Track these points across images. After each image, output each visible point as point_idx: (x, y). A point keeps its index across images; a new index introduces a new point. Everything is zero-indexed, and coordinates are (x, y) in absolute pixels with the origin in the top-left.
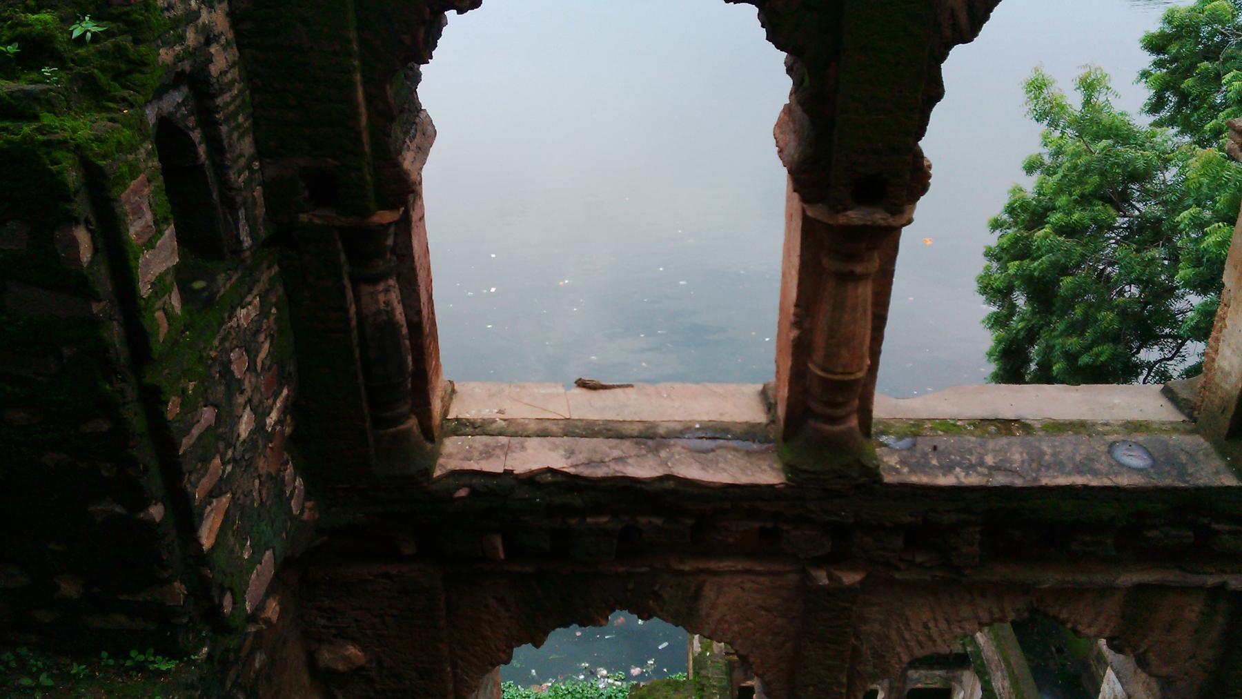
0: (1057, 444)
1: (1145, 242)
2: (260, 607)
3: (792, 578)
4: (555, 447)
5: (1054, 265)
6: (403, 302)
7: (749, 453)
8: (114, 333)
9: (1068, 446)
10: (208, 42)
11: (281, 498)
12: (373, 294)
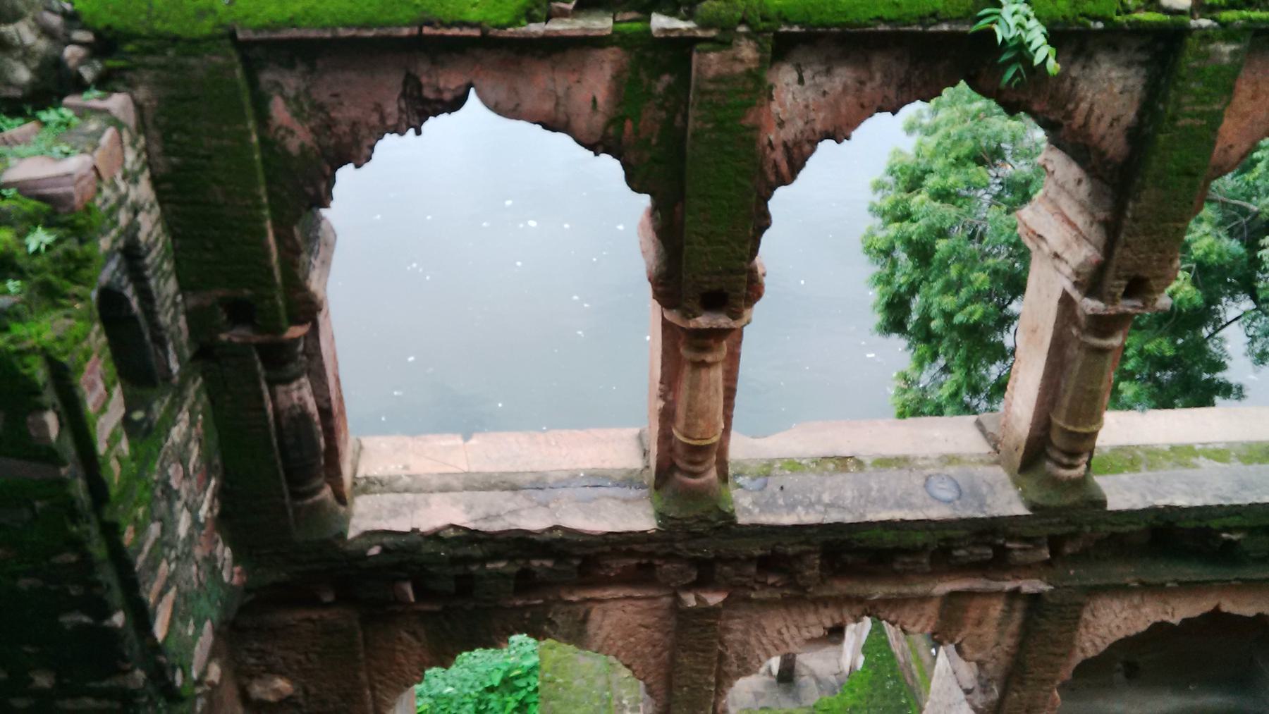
0: (883, 479)
1: (1014, 203)
2: (204, 673)
3: (666, 601)
4: (456, 503)
5: (930, 228)
6: (315, 393)
7: (626, 501)
8: (79, 488)
9: (895, 481)
10: (136, 213)
11: (215, 572)
12: (287, 393)
